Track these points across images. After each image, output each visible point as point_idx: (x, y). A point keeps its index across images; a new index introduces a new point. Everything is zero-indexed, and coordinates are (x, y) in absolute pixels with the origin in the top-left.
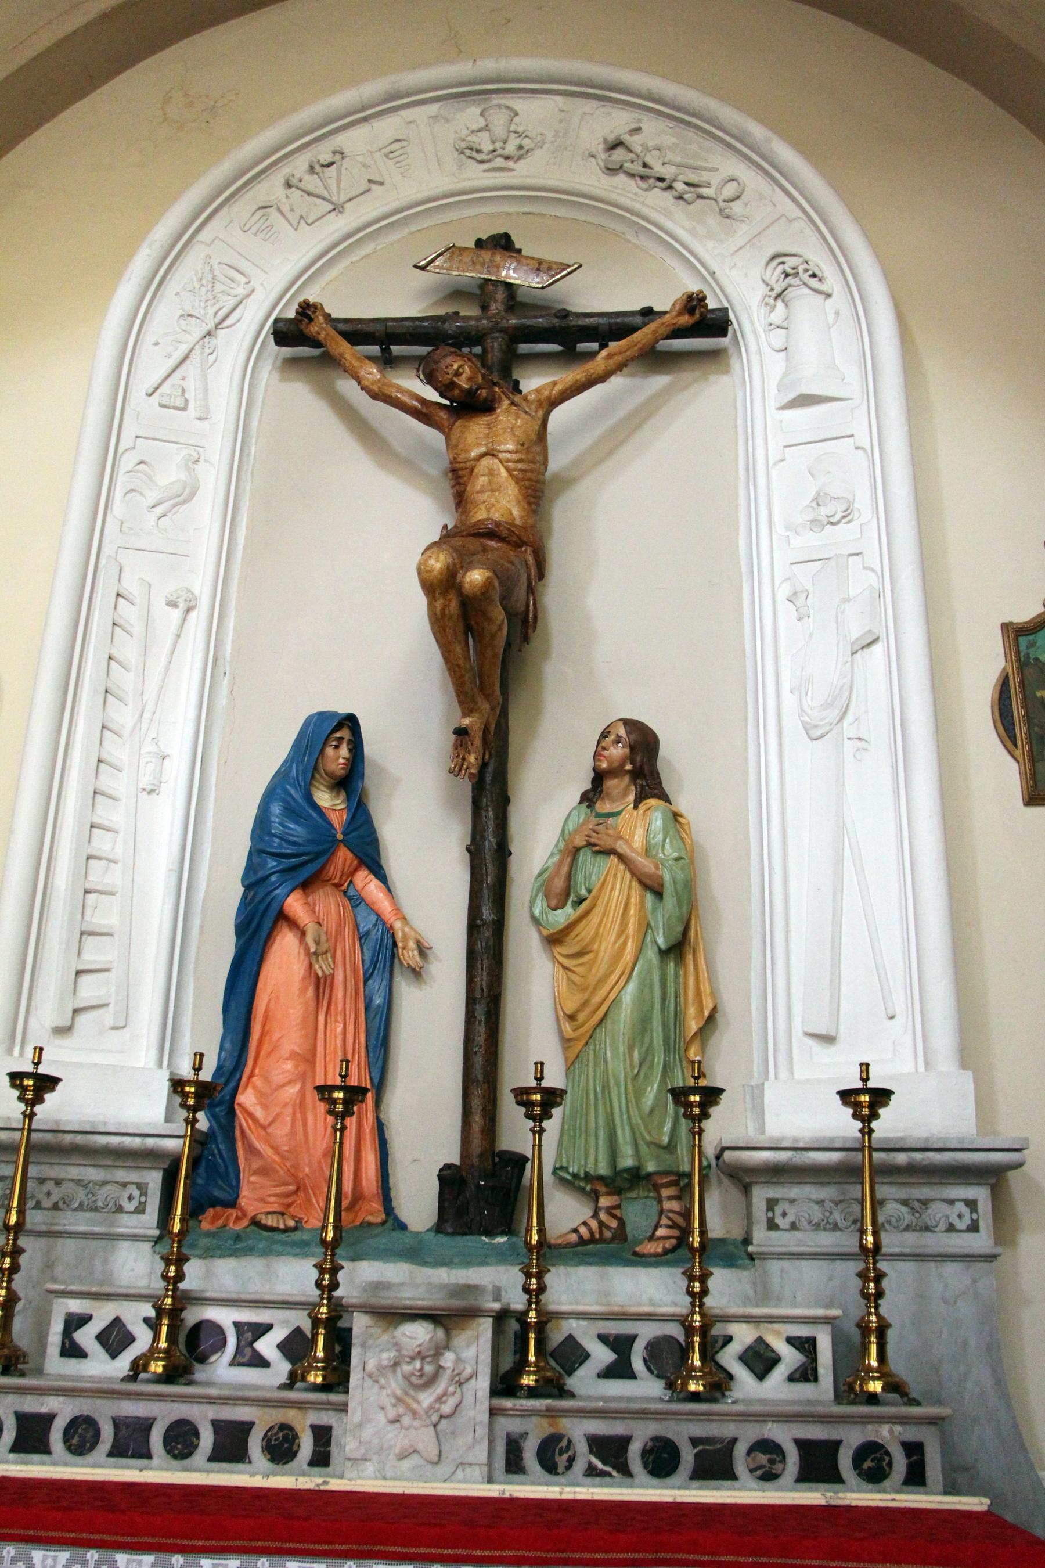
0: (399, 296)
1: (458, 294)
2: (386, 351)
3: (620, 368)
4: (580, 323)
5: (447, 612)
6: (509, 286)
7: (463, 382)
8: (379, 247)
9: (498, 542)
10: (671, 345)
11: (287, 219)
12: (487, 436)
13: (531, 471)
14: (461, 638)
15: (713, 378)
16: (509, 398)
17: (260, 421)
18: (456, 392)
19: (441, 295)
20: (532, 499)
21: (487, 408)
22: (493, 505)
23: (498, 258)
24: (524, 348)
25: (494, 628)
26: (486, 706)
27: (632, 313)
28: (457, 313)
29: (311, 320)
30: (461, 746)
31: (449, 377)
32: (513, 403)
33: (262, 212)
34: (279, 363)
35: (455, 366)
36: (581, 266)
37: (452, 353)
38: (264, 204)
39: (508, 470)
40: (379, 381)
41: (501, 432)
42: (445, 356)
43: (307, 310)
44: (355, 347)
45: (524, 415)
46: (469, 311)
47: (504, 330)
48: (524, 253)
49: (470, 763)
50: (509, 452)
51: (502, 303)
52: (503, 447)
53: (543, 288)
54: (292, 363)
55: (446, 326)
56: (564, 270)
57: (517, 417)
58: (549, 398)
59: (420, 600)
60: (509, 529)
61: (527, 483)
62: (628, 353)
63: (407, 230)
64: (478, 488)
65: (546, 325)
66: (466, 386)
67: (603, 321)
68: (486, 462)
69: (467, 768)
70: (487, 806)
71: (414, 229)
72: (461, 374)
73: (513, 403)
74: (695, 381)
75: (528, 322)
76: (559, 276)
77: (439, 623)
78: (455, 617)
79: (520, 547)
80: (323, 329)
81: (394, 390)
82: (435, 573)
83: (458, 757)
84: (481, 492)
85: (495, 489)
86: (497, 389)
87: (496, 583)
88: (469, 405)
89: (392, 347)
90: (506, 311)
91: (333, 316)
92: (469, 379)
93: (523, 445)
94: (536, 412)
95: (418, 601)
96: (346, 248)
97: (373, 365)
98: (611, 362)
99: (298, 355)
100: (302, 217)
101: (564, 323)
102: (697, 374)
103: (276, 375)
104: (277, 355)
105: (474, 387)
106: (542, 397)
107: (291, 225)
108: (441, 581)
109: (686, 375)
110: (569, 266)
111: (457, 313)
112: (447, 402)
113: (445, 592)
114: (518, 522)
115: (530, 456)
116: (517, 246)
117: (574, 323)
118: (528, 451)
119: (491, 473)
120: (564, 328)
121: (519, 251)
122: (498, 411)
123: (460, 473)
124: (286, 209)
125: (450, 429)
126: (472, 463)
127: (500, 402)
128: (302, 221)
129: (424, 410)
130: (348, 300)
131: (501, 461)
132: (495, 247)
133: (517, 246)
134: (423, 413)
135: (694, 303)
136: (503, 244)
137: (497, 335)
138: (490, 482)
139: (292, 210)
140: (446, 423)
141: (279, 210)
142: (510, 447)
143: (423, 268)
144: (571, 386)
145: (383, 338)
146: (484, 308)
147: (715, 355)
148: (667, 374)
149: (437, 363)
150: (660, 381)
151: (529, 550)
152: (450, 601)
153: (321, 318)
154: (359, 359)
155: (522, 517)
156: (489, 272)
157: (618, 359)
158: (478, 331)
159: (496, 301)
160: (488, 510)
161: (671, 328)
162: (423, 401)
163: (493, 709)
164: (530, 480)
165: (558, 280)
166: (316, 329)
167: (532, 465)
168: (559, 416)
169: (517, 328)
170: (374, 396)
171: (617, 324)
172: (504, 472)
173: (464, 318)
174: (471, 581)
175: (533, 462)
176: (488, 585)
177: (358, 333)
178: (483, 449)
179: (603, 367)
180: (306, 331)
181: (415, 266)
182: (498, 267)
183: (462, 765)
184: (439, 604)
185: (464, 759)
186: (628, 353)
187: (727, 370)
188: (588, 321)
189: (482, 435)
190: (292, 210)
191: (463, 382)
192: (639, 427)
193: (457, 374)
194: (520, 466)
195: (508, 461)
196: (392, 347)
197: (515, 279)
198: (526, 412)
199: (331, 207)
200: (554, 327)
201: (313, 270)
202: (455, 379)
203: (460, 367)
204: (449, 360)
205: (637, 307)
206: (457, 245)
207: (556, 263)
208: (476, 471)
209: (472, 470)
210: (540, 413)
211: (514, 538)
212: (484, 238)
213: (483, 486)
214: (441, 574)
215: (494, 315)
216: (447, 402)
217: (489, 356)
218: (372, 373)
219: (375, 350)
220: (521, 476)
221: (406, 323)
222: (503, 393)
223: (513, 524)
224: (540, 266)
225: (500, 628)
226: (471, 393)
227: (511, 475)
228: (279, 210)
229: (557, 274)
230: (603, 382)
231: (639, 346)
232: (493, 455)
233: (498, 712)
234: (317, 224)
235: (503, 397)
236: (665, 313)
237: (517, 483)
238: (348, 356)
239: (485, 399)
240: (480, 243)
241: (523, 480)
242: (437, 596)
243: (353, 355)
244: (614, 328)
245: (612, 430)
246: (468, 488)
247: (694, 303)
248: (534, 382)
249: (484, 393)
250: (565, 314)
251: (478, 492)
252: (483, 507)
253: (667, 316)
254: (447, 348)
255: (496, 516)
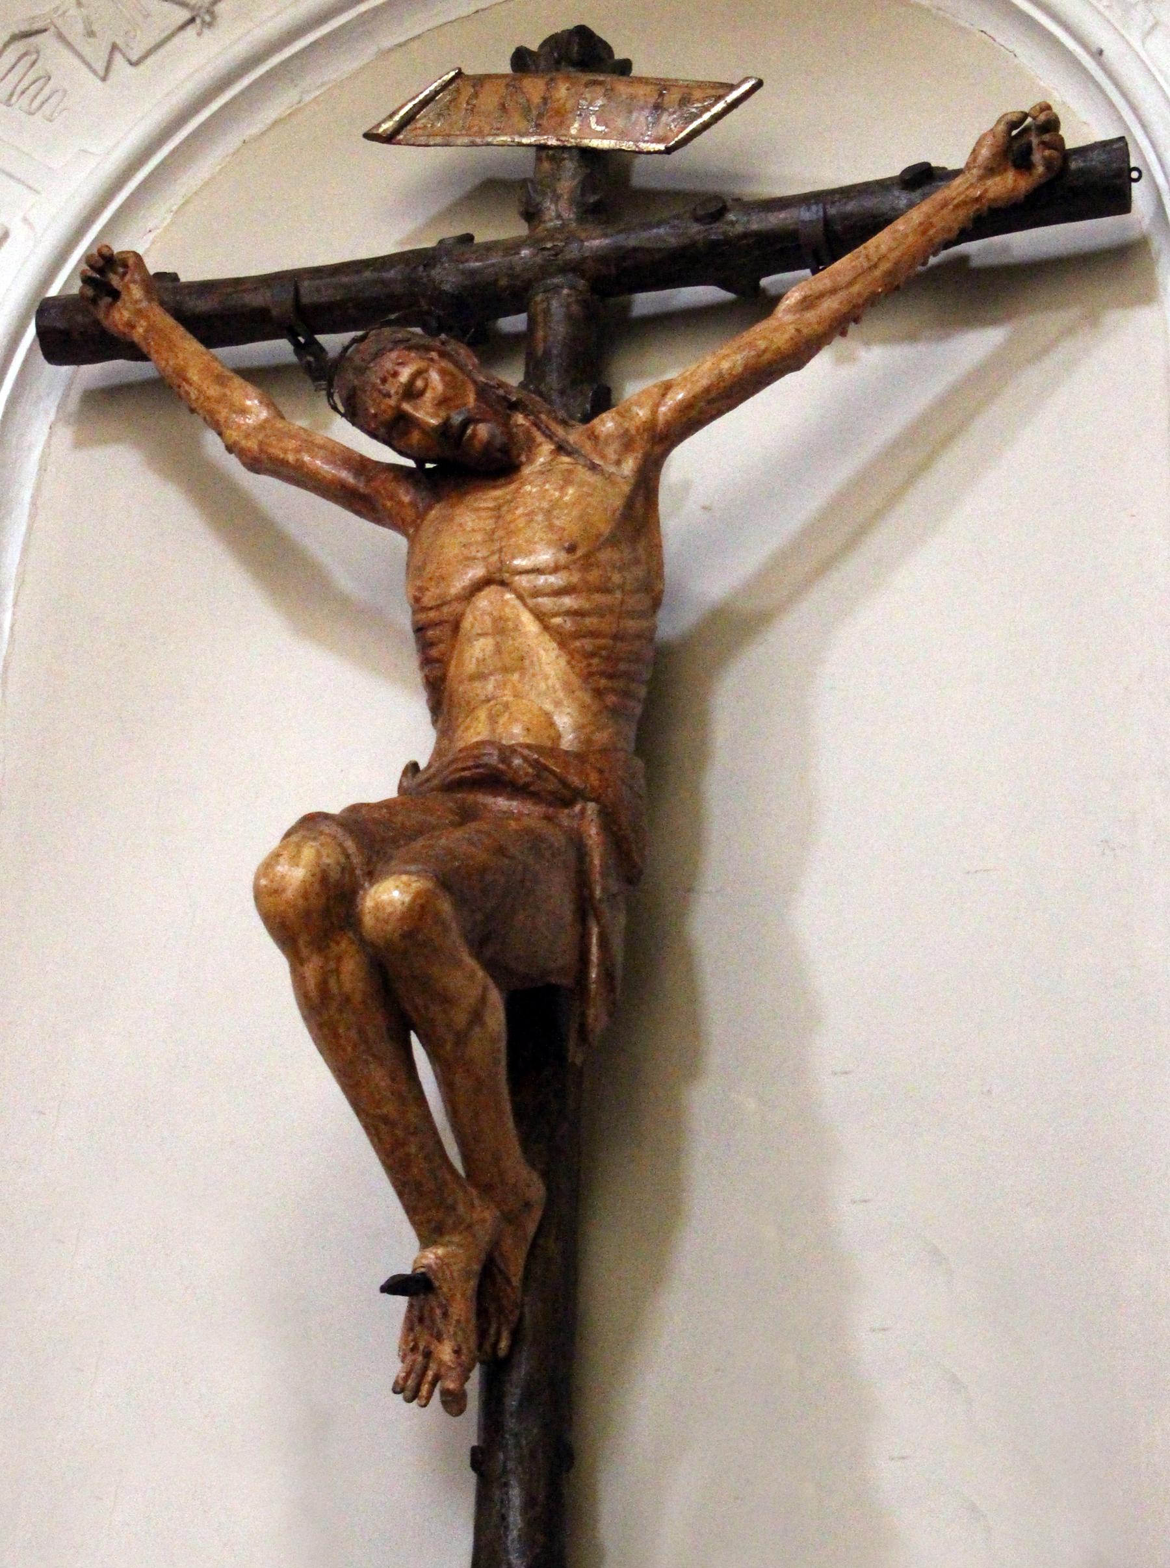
0: (352, 209)
1: (490, 190)
2: (307, 349)
3: (839, 326)
4: (755, 227)
5: (332, 982)
6: (589, 155)
7: (427, 414)
8: (308, 98)
9: (510, 797)
10: (1006, 249)
11: (79, 55)
12: (490, 536)
13: (599, 611)
14: (386, 1048)
15: (1113, 317)
16: (550, 437)
17: (25, 550)
18: (416, 436)
19: (458, 193)
20: (603, 682)
21: (499, 466)
22: (506, 706)
23: (562, 91)
24: (645, 302)
25: (461, 1018)
26: (485, 1216)
27: (883, 185)
28: (469, 238)
29: (115, 295)
30: (421, 1320)
31: (392, 402)
32: (561, 448)
33: (20, 47)
34: (73, 404)
35: (405, 375)
36: (759, 84)
37: (397, 343)
38: (24, 27)
39: (540, 616)
40: (262, 427)
41: (521, 523)
42: (379, 354)
43: (106, 271)
44: (213, 351)
45: (583, 474)
46: (498, 228)
47: (575, 268)
48: (636, 71)
49: (441, 1363)
50: (537, 571)
51: (572, 201)
52: (520, 563)
53: (669, 151)
54: (102, 402)
55: (436, 273)
56: (719, 98)
57: (567, 481)
58: (650, 426)
59: (275, 964)
60: (536, 764)
61: (588, 644)
62: (855, 289)
63: (375, 48)
64: (471, 667)
65: (673, 241)
66: (434, 422)
67: (807, 214)
68: (484, 601)
69: (437, 1378)
70: (505, 1471)
71: (387, 42)
72: (421, 393)
73: (561, 448)
74: (1069, 332)
75: (632, 240)
76: (706, 117)
77: (321, 1010)
78: (357, 998)
79: (568, 803)
80: (139, 313)
81: (292, 444)
82: (289, 894)
83: (414, 1349)
84: (481, 676)
85: (517, 663)
86: (520, 419)
87: (445, 906)
88: (458, 466)
89: (321, 338)
90: (581, 220)
91: (184, 278)
92: (443, 402)
93: (571, 549)
94: (618, 463)
95: (270, 973)
96: (214, 116)
97: (250, 389)
98: (811, 316)
99: (115, 381)
100: (114, 47)
101: (717, 231)
102: (1075, 312)
103: (66, 434)
104: (69, 387)
105: (457, 419)
106: (632, 426)
107: (95, 72)
108: (307, 913)
109: (1044, 321)
110: (732, 87)
111: (469, 238)
112: (410, 463)
113: (321, 943)
114: (568, 741)
115: (594, 576)
116: (619, 55)
117: (739, 229)
118: (587, 563)
119: (501, 628)
120: (715, 244)
121: (624, 67)
122: (526, 471)
123: (430, 633)
124: (75, 32)
125: (418, 528)
126: (457, 607)
127: (530, 447)
128: (118, 59)
129: (362, 487)
130: (198, 239)
131: (520, 597)
132: (557, 65)
133: (619, 55)
134: (360, 493)
135: (1027, 139)
136: (582, 54)
137: (557, 280)
138: (498, 650)
139: (91, 34)
140: (410, 514)
141: (61, 37)
142: (545, 556)
143: (389, 139)
144: (707, 390)
145: (297, 321)
146: (531, 215)
147: (1122, 263)
148: (994, 322)
149: (361, 371)
150: (977, 344)
151: (591, 807)
152: (339, 959)
153: (137, 292)
154: (220, 380)
155: (579, 728)
156: (539, 129)
157: (830, 305)
158: (512, 276)
159: (557, 198)
160: (493, 719)
161: (971, 210)
162: (362, 466)
163: (511, 1218)
164: (593, 634)
165: (706, 126)
166: (126, 315)
167: (599, 598)
168: (695, 465)
169: (602, 258)
170: (256, 463)
171: (845, 217)
172: (530, 625)
173: (489, 247)
174: (378, 907)
175: (604, 589)
176: (420, 912)
177: (221, 314)
178: (476, 572)
179: (791, 331)
180: (106, 323)
181: (369, 136)
182: (561, 117)
183: (425, 1368)
184: (311, 970)
185: (428, 1355)
186: (855, 289)
187: (1147, 295)
188: (776, 220)
189: (479, 537)
190: (91, 34)
191: (427, 414)
192: (925, 466)
193: (411, 393)
194: (568, 602)
195: (536, 593)
196: (321, 338)
197: (604, 136)
198: (593, 467)
199: (185, 15)
200: (693, 244)
201: (147, 172)
202: (407, 407)
203: (418, 374)
204: (388, 362)
205: (894, 169)
206: (467, 71)
207: (701, 85)
208: (466, 624)
209: (456, 626)
210: (629, 466)
211: (552, 785)
212: (534, 47)
213: (481, 661)
214: (305, 896)
215: (551, 234)
216: (410, 463)
217: (540, 334)
218: (254, 409)
219: (279, 349)
220: (569, 625)
221: (368, 274)
222: (536, 425)
223: (553, 751)
224: (665, 95)
225: (477, 1017)
226: (450, 435)
227: (546, 628)
228: (61, 37)
229: (707, 109)
230: (798, 367)
231: (885, 266)
232: (503, 583)
233: (531, 1228)
234: (149, 61)
235: (540, 438)
236: (957, 173)
237: (562, 645)
238: (194, 375)
239: (488, 445)
240: (522, 60)
241: (577, 635)
242: (305, 952)
243: (206, 370)
244: (834, 227)
245: (863, 480)
246: (452, 670)
247: (1027, 139)
248: (650, 383)
249: (483, 431)
250: (715, 208)
251: (474, 677)
252: (482, 714)
253: (958, 181)
254: (387, 331)
255: (515, 733)
